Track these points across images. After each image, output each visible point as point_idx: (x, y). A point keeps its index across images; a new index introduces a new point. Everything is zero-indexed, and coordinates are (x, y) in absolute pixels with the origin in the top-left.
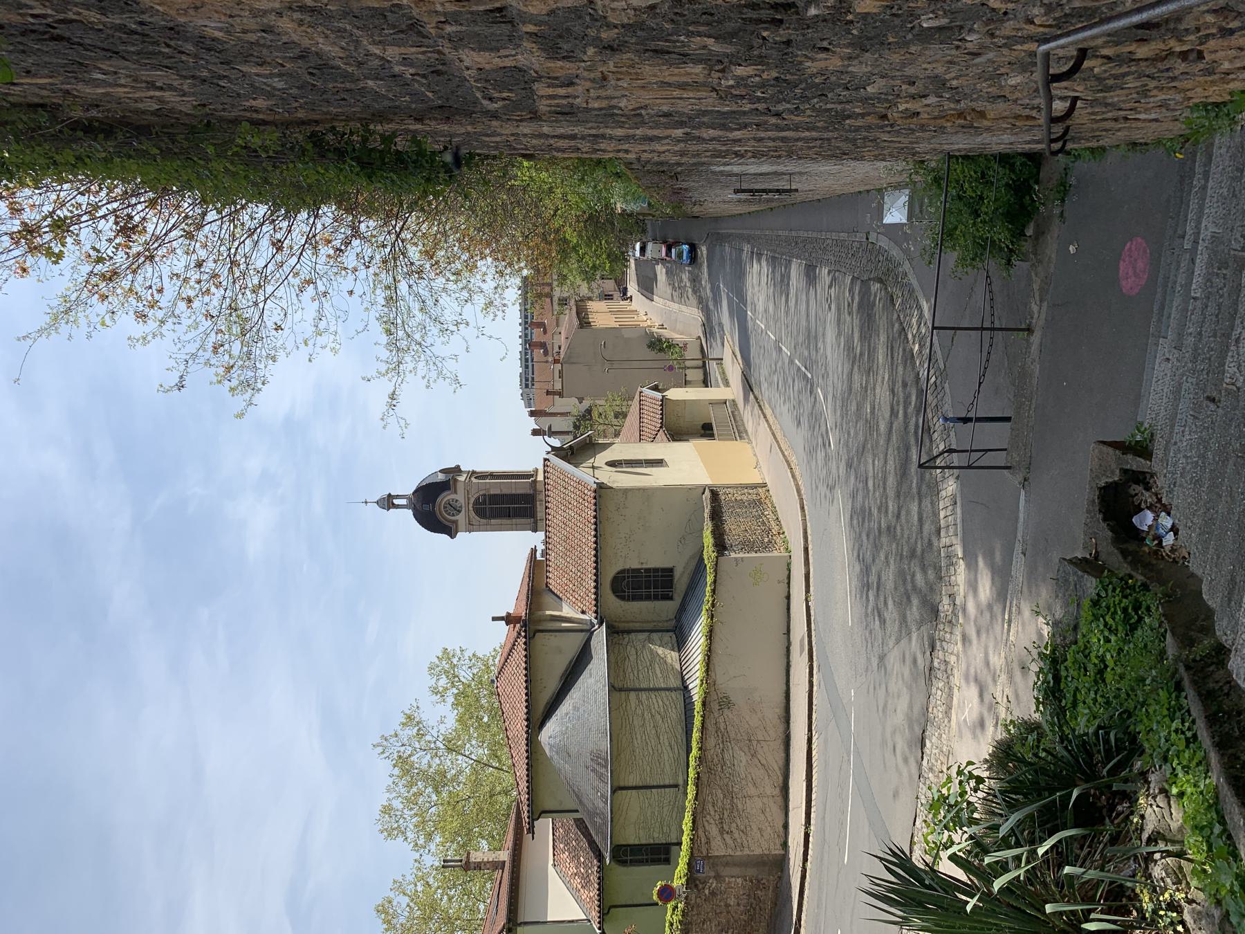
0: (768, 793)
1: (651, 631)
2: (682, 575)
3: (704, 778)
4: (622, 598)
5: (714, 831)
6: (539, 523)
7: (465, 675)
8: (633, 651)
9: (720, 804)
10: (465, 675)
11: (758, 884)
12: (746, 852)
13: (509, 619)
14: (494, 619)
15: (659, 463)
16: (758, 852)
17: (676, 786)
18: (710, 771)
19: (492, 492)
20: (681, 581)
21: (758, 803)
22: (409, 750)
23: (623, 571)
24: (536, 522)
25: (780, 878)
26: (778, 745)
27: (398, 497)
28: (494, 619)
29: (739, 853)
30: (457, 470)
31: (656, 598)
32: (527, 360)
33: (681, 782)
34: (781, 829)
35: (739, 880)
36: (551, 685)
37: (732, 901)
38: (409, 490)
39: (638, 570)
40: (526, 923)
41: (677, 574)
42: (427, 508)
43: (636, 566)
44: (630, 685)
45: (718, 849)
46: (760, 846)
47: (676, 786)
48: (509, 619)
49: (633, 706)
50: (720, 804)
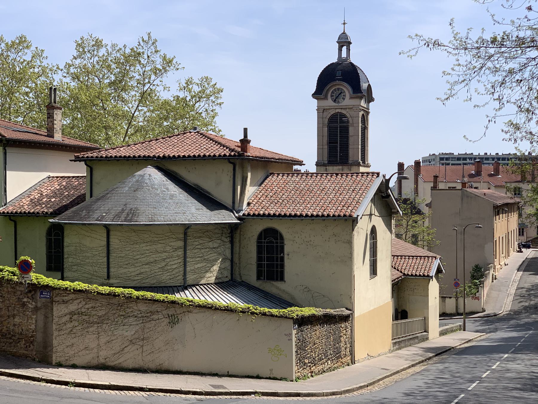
0: (101, 353)
1: (232, 261)
2: (278, 288)
3: (115, 300)
4: (260, 237)
5: (73, 307)
6: (323, 168)
7: (201, 106)
8: (216, 245)
9: (94, 313)
11: (30, 341)
12: (55, 333)
13: (245, 142)
14: (245, 130)
15: (374, 272)
16: (55, 342)
17: (108, 277)
18: (120, 305)
20: (274, 287)
21: (93, 345)
24: (324, 165)
25: (34, 360)
27: (348, 50)
28: (245, 130)
29: (54, 327)
31: (259, 266)
32: (465, 159)
34: (71, 363)
35: (33, 327)
37: (17, 320)
38: (354, 59)
39: (282, 251)
40: (5, 154)
41: (279, 284)
42: (339, 73)
43: (287, 249)
45: (59, 310)
47: (108, 277)
48: (245, 142)
49: (173, 244)
50: (94, 313)
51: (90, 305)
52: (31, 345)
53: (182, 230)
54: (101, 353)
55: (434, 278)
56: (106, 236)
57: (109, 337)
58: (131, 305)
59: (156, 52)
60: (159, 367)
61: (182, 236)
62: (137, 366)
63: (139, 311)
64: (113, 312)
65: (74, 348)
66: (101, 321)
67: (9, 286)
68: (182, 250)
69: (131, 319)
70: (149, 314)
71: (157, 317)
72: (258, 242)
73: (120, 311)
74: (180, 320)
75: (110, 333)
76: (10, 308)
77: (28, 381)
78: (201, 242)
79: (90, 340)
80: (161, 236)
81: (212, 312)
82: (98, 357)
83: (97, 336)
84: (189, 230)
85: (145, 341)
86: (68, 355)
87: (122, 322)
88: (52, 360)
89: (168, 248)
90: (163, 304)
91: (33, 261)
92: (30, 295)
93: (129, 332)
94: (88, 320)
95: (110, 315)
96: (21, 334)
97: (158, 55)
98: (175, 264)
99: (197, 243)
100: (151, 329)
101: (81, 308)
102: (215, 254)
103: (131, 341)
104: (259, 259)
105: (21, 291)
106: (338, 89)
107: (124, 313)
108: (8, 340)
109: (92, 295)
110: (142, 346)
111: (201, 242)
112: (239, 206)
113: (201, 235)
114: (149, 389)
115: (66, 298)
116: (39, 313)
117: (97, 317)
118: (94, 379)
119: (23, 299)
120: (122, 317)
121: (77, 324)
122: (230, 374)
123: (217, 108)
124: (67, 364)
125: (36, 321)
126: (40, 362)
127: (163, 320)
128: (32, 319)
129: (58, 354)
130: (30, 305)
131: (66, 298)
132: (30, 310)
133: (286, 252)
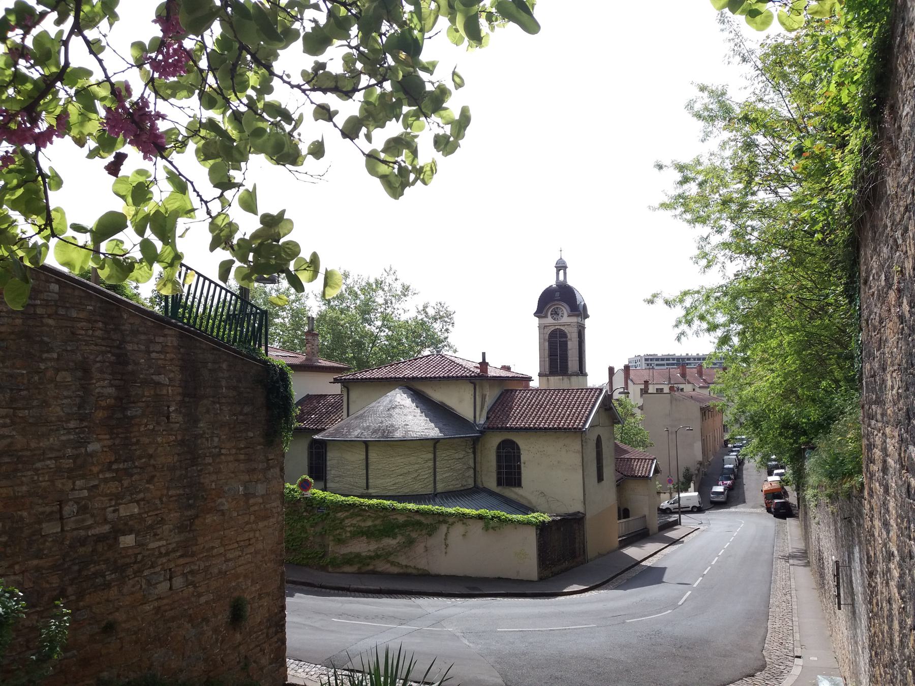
1: (475, 469)
2: (516, 493)
4: (499, 447)
6: (545, 378)
7: (437, 326)
8: (461, 456)
10: (437, 326)
13: (484, 365)
14: (484, 354)
15: (600, 478)
17: (367, 487)
19: (569, 343)
20: (511, 493)
22: (386, 288)
23: (519, 449)
24: (546, 375)
27: (565, 274)
28: (484, 354)
30: (587, 316)
31: (499, 473)
32: (668, 359)
33: (370, 491)
36: (438, 395)
38: (570, 282)
39: (520, 461)
41: (517, 490)
43: (523, 458)
44: (438, 453)
47: (367, 487)
48: (484, 365)
53: (432, 443)
55: (321, 59)
59: (396, 279)
72: (497, 452)
89: (420, 461)
98: (224, 334)
104: (499, 467)
123: (450, 327)
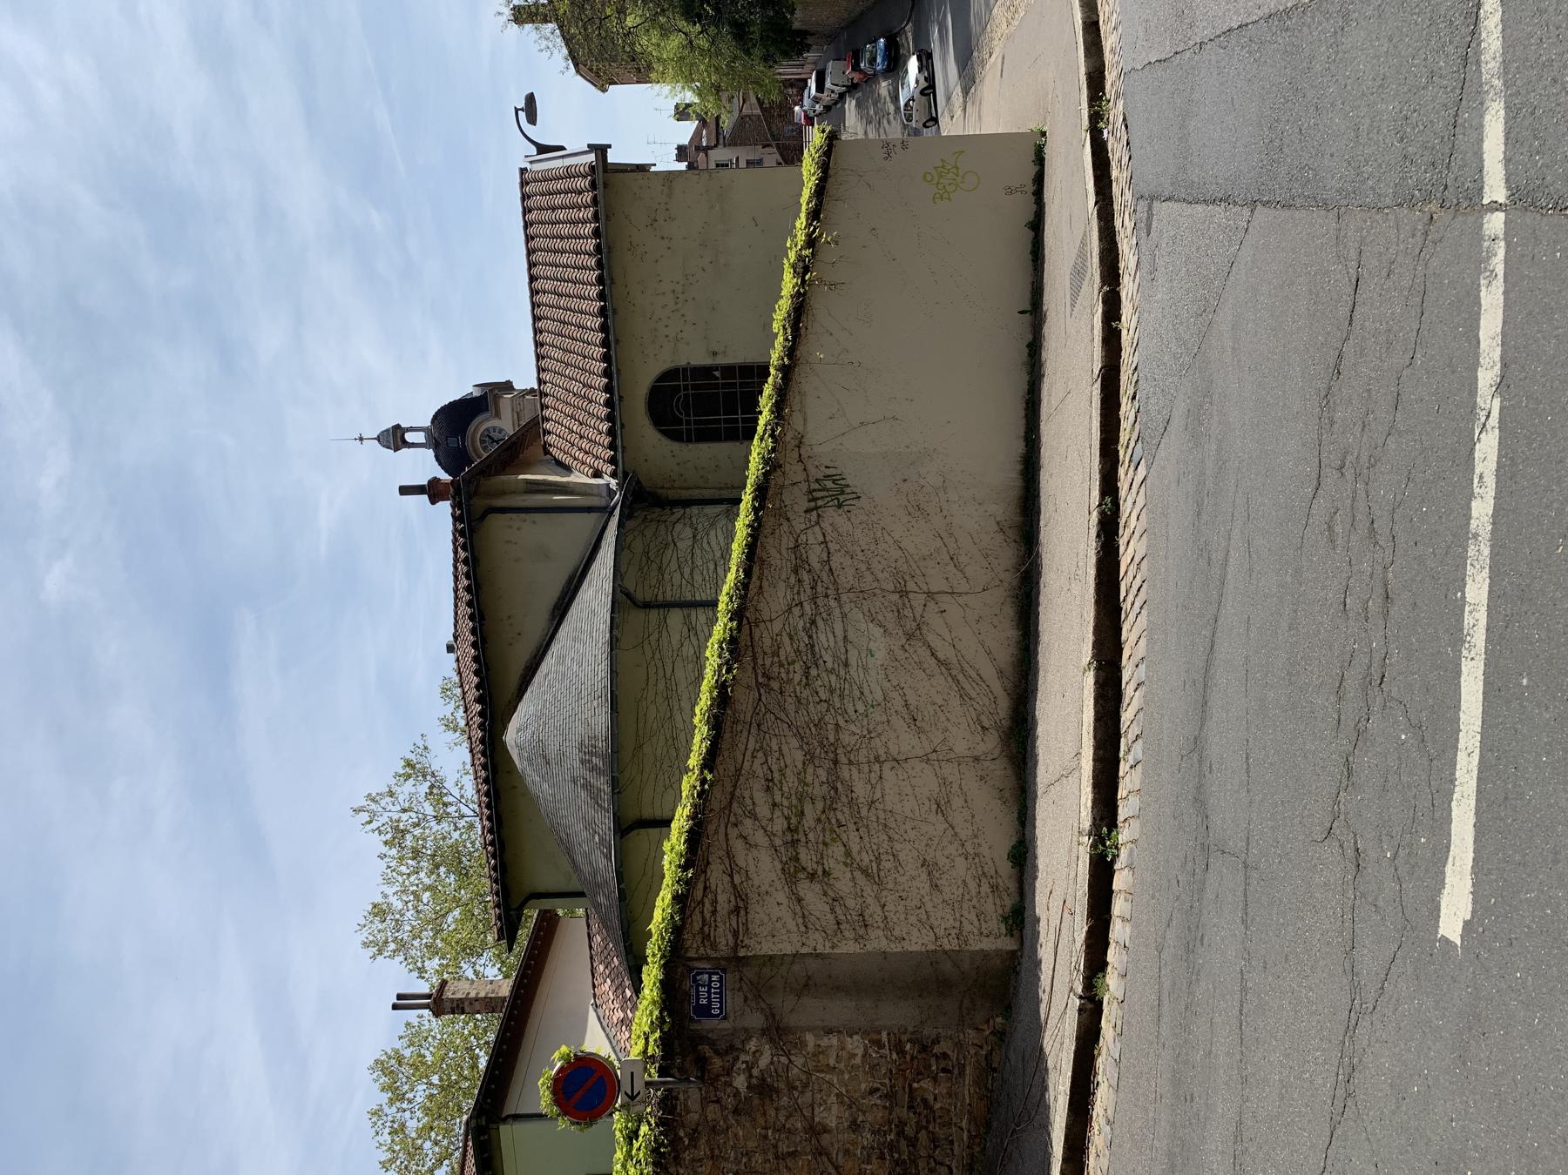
0: (961, 748)
3: (744, 700)
4: (675, 436)
5: (763, 868)
8: (688, 532)
9: (791, 781)
11: (918, 1055)
12: (878, 942)
13: (433, 491)
14: (405, 490)
16: (918, 942)
18: (765, 680)
21: (926, 781)
23: (670, 374)
25: (1001, 1036)
26: (997, 606)
28: (405, 490)
29: (848, 947)
34: (1006, 868)
35: (856, 1044)
37: (832, 1116)
39: (706, 371)
40: (517, 1117)
42: (453, 442)
43: (700, 359)
45: (776, 930)
46: (926, 924)
49: (675, 639)
50: (791, 781)
51: (760, 797)
52: (937, 1049)
54: (961, 748)
56: (657, 830)
57: (894, 719)
58: (767, 642)
59: (391, 794)
60: (1012, 534)
61: (654, 615)
62: (1009, 611)
63: (790, 610)
64: (791, 708)
65: (942, 861)
66: (828, 754)
67: (687, 1156)
68: (693, 612)
69: (823, 638)
70: (805, 577)
71: (818, 549)
72: (689, 441)
73: (790, 681)
74: (829, 472)
75: (877, 715)
76: (783, 1148)
77: (1100, 1063)
78: (674, 566)
79: (905, 793)
80: (652, 670)
81: (800, 374)
82: (976, 759)
83: (887, 766)
84: (639, 597)
85: (911, 586)
86: (972, 885)
87: (832, 671)
88: (998, 952)
90: (767, 530)
91: (557, 1055)
92: (717, 1063)
93: (872, 646)
94: (820, 805)
95: (802, 719)
96: (890, 1096)
97: (399, 790)
99: (677, 576)
100: (863, 567)
101: (770, 835)
102: (712, 533)
103: (910, 637)
105: (705, 1101)
106: (482, 442)
107: (797, 666)
108: (923, 1153)
109: (717, 792)
110: (929, 593)
111: (674, 566)
112: (599, 495)
113: (654, 566)
114: (1103, 494)
115: (724, 900)
116: (792, 1020)
117: (810, 770)
118: (1069, 750)
119: (737, 1094)
120: (814, 672)
121: (837, 850)
122: (1028, 307)
124: (1013, 886)
125: (829, 1031)
126: (1009, 1008)
127: (829, 529)
128: (820, 1052)
129: (967, 927)
130: (764, 1062)
131: (724, 900)
132: (784, 1060)
133: (708, 361)
